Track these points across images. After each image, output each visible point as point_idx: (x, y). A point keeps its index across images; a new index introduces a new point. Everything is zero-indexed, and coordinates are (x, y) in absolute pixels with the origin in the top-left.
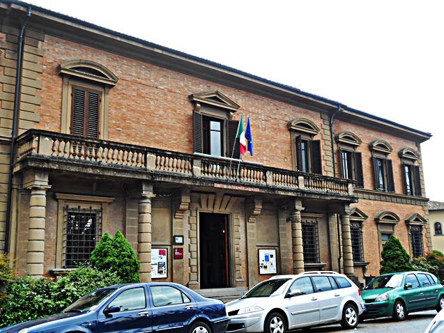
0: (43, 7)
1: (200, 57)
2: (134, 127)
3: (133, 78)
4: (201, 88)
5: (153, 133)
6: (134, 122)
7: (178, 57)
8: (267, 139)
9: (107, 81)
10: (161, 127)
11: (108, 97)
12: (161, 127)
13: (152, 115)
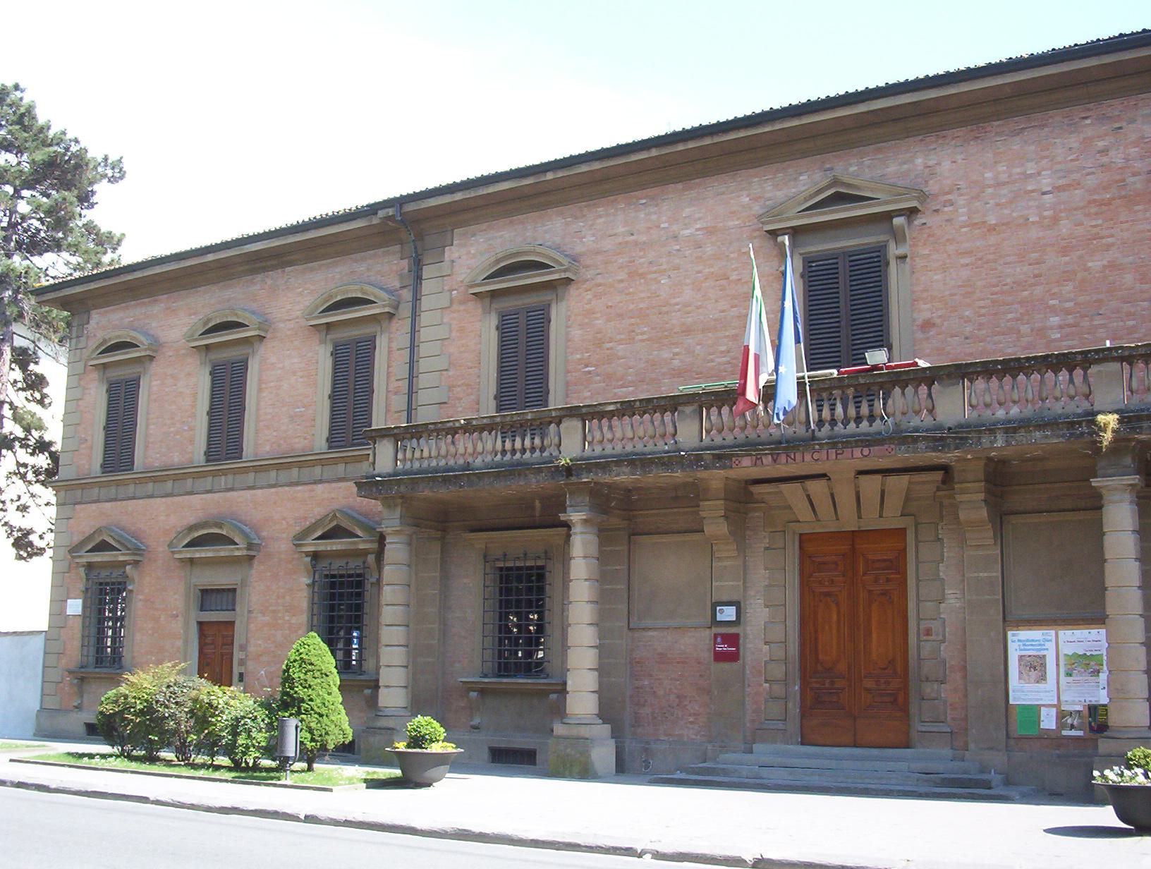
0: (431, 187)
1: (537, 163)
2: (620, 354)
3: (620, 240)
4: (792, 187)
5: (666, 355)
6: (620, 342)
7: (778, 126)
8: (1065, 251)
9: (879, 205)
10: (687, 331)
11: (563, 306)
12: (687, 331)
13: (664, 309)
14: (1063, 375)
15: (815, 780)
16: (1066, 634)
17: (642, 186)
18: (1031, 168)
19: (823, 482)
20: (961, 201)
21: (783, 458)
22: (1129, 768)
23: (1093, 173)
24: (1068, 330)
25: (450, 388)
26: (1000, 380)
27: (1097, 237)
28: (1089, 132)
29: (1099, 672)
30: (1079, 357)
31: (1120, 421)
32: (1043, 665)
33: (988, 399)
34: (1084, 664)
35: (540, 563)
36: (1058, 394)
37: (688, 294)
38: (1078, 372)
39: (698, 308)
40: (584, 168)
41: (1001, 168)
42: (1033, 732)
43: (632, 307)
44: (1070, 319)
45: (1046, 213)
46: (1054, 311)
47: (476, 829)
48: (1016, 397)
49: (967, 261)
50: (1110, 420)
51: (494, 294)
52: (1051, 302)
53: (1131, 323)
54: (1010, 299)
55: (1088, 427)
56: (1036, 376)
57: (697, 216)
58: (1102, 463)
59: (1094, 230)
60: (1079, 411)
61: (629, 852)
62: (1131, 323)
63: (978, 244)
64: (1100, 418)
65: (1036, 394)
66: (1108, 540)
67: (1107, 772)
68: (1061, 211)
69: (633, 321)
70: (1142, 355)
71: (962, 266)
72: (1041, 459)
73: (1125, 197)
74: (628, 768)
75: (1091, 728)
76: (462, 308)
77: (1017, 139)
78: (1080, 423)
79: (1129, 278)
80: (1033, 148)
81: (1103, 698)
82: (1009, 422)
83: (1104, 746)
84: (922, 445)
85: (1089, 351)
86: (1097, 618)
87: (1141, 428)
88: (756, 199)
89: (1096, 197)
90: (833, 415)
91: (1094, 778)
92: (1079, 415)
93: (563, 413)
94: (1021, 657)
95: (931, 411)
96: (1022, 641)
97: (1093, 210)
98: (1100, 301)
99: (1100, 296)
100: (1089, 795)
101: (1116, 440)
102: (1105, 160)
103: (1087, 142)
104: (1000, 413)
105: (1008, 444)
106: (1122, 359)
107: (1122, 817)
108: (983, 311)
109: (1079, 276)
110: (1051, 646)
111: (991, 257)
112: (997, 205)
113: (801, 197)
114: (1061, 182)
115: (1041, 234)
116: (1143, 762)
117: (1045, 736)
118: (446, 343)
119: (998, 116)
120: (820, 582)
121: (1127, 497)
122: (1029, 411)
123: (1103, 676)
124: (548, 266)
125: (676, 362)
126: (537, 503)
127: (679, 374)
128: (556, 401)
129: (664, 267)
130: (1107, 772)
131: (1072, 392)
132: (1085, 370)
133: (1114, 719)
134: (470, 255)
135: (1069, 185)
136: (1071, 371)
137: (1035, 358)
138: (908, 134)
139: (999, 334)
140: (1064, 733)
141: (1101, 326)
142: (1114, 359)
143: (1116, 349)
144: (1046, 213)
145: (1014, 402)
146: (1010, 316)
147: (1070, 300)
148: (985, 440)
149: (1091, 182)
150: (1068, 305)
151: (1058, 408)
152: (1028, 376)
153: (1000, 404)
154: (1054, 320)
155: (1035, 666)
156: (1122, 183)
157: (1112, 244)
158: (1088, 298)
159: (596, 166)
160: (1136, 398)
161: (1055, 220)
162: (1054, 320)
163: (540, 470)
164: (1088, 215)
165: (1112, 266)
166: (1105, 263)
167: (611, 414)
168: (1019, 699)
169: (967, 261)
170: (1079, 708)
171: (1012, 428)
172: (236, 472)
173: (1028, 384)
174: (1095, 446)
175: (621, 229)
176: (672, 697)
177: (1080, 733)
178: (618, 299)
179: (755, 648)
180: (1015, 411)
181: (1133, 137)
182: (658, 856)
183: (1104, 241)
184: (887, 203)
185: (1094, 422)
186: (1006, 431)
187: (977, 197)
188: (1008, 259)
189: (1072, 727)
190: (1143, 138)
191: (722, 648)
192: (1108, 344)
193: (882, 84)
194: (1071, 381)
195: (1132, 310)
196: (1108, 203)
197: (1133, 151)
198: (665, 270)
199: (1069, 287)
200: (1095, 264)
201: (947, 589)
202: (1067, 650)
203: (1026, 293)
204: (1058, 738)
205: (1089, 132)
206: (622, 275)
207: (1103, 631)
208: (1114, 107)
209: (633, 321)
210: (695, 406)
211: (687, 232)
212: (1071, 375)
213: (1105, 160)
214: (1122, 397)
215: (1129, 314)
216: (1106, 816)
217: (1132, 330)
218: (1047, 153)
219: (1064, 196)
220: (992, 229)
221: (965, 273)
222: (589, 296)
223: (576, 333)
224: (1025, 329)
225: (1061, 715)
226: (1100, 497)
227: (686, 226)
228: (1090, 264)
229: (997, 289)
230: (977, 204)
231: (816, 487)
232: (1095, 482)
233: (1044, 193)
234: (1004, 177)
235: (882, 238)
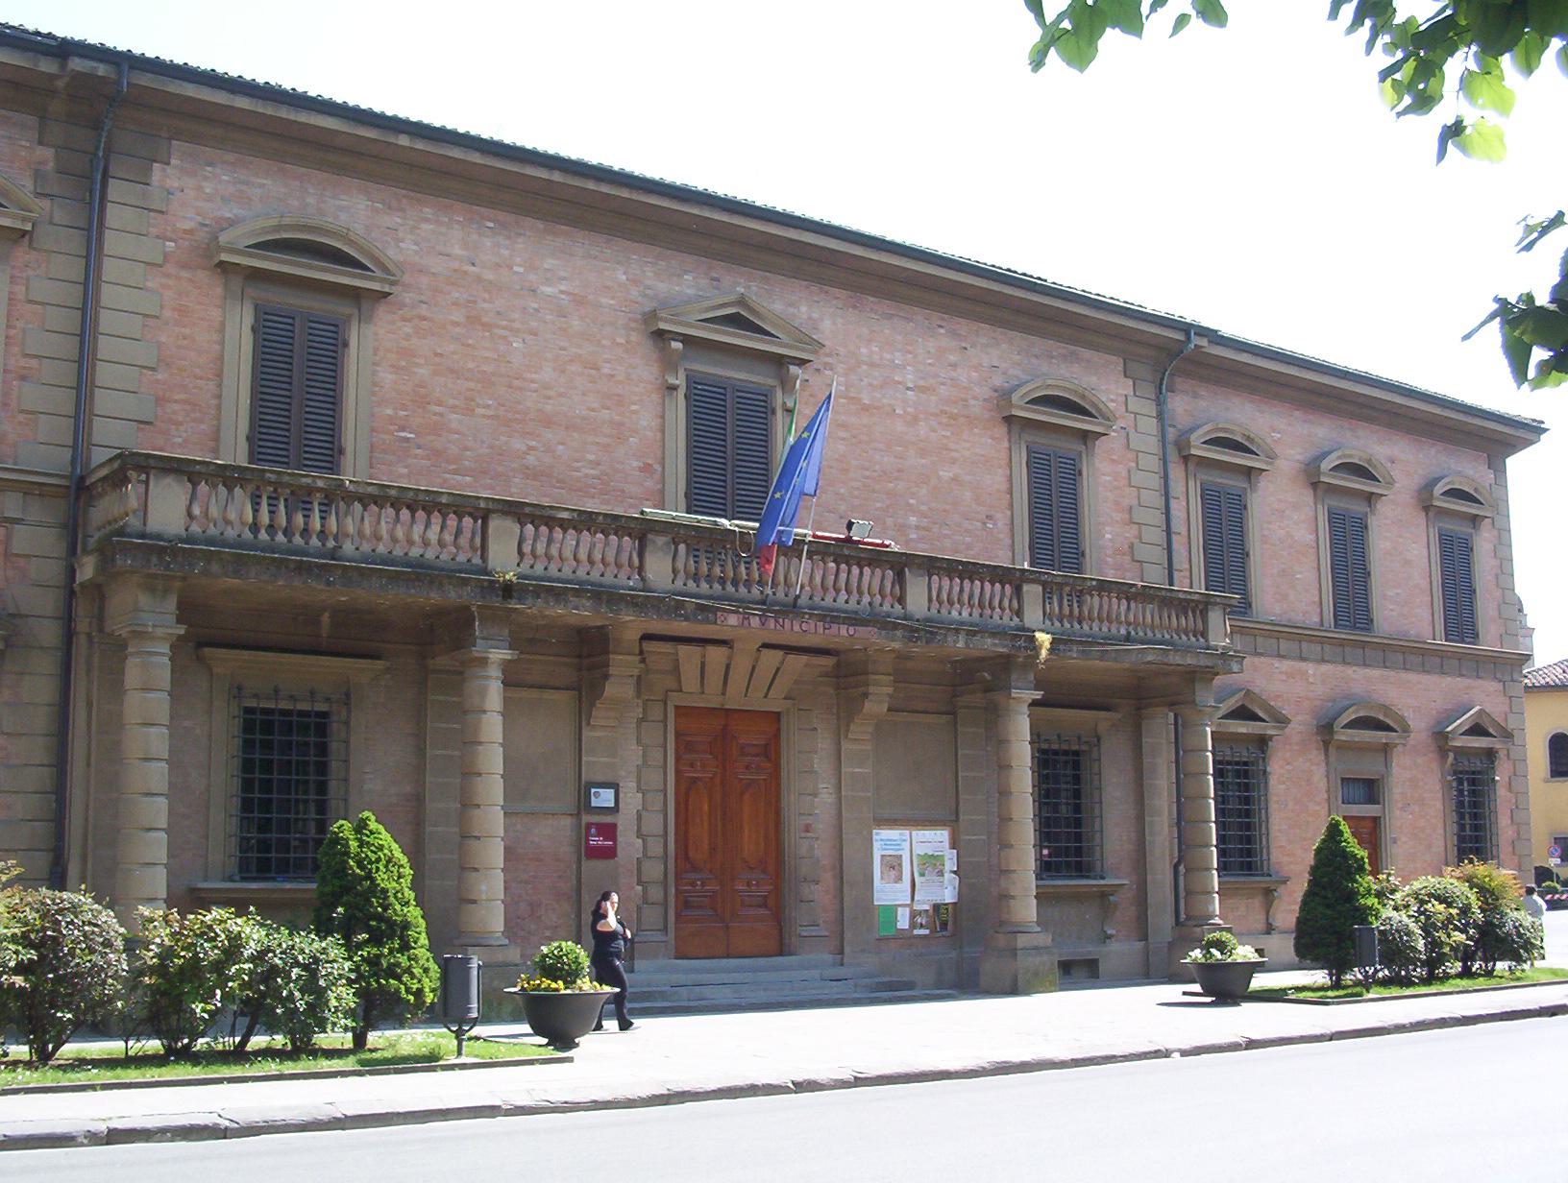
2: (454, 425)
3: (456, 265)
4: (691, 289)
5: (518, 444)
6: (453, 408)
7: (605, 189)
12: (548, 422)
13: (516, 383)
15: (762, 996)
17: (492, 204)
19: (723, 650)
21: (772, 623)
25: (160, 401)
35: (322, 707)
37: (547, 373)
39: (561, 395)
40: (456, 153)
42: (892, 932)
43: (471, 365)
44: (925, 522)
47: (761, 1080)
49: (842, 434)
51: (256, 275)
57: (563, 274)
61: (1157, 1054)
69: (472, 385)
74: (1079, 972)
76: (184, 274)
84: (899, 633)
88: (635, 282)
93: (496, 507)
95: (901, 600)
96: (887, 840)
113: (709, 304)
114: (922, 383)
118: (150, 322)
119: (875, 293)
120: (692, 765)
125: (531, 459)
126: (326, 618)
127: (533, 474)
128: (353, 472)
129: (517, 325)
134: (205, 196)
140: (916, 932)
154: (913, 520)
159: (476, 158)
161: (916, 419)
162: (913, 520)
163: (895, 626)
165: (955, 479)
167: (564, 525)
169: (842, 434)
170: (927, 907)
175: (457, 251)
176: (523, 905)
178: (452, 347)
179: (628, 843)
182: (1184, 1053)
184: (786, 346)
191: (596, 841)
193: (461, 130)
198: (518, 330)
199: (924, 491)
200: (945, 474)
201: (818, 780)
206: (458, 316)
208: (963, 326)
209: (472, 385)
210: (668, 538)
211: (549, 290)
217: (969, 547)
220: (866, 408)
221: (842, 448)
222: (408, 329)
223: (387, 377)
225: (914, 914)
227: (548, 282)
231: (716, 654)
235: (770, 382)
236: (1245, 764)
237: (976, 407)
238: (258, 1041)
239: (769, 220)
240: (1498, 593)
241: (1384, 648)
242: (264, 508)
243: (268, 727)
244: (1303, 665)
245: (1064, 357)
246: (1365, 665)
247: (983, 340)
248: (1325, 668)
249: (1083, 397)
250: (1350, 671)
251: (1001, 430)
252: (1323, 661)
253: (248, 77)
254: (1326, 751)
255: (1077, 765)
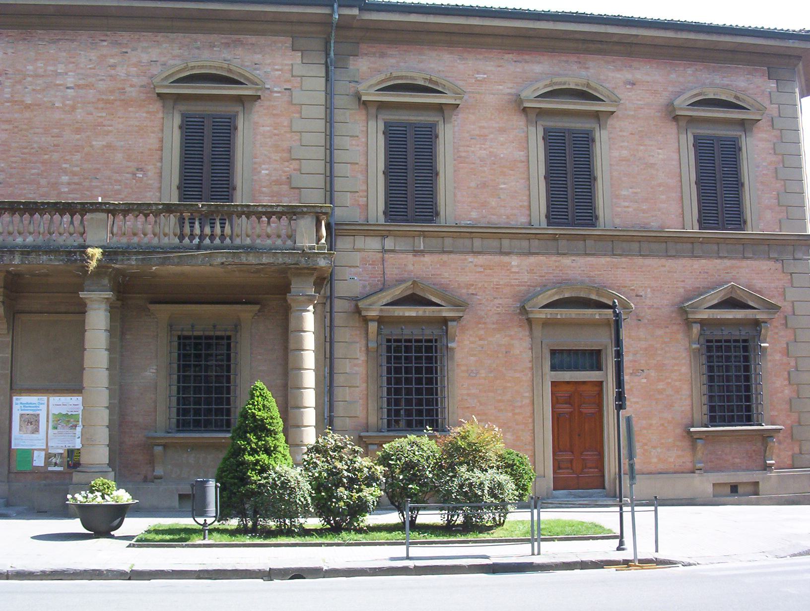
8: (78, 131)
14: (67, 218)
16: (55, 400)
18: (61, 68)
20: (8, 83)
22: (92, 492)
23: (103, 80)
24: (73, 186)
26: (21, 216)
27: (101, 125)
28: (105, 51)
29: (76, 426)
30: (79, 207)
31: (103, 254)
32: (38, 421)
33: (11, 229)
34: (66, 421)
35: (228, 333)
36: (61, 230)
38: (77, 217)
41: (40, 64)
42: (28, 468)
45: (68, 102)
46: (65, 171)
48: (32, 230)
50: (96, 253)
52: (64, 166)
53: (119, 187)
54: (34, 159)
55: (81, 256)
56: (47, 216)
58: (87, 282)
59: (100, 120)
60: (76, 244)
62: (119, 187)
63: (16, 115)
64: (90, 250)
65: (46, 229)
66: (88, 335)
67: (77, 495)
68: (78, 102)
70: (122, 211)
71: (3, 130)
72: (47, 275)
73: (123, 100)
75: (69, 466)
77: (54, 46)
78: (75, 253)
79: (119, 156)
80: (64, 54)
81: (78, 445)
82: (25, 247)
83: (77, 477)
85: (87, 203)
86: (76, 388)
87: (117, 260)
89: (103, 97)
90: (192, 231)
91: (68, 500)
92: (75, 247)
94: (22, 415)
96: (23, 404)
97: (101, 105)
98: (99, 169)
99: (99, 166)
100: (64, 512)
101: (98, 267)
102: (113, 72)
103: (103, 57)
104: (19, 240)
105: (23, 262)
106: (108, 211)
107: (85, 526)
108: (14, 165)
109: (87, 149)
110: (44, 408)
111: (25, 127)
112: (34, 90)
114: (81, 82)
115: (63, 116)
116: (101, 488)
117: (36, 471)
121: (103, 306)
122: (40, 240)
123: (79, 429)
124: (242, 83)
128: (241, 198)
130: (77, 495)
131: (72, 229)
132: (82, 216)
133: (84, 459)
135: (87, 86)
136: (72, 216)
137: (48, 203)
138: (159, 30)
139: (24, 183)
140: (50, 469)
141: (97, 187)
142: (103, 211)
143: (106, 204)
144: (68, 102)
145: (30, 233)
146: (33, 171)
147: (77, 166)
148: (6, 259)
149: (101, 85)
150: (76, 169)
151: (61, 240)
152: (41, 215)
153: (20, 233)
154: (65, 178)
155: (31, 422)
156: (122, 91)
157: (111, 132)
158: (90, 166)
160: (115, 239)
161: (73, 108)
162: (65, 178)
164: (97, 108)
165: (109, 146)
166: (104, 143)
168: (18, 445)
171: (27, 251)
172: (424, 234)
173: (42, 221)
174: (84, 269)
177: (61, 469)
180: (30, 239)
181: (134, 60)
183: (106, 128)
185: (84, 252)
186: (22, 253)
187: (20, 82)
188: (37, 131)
189: (56, 464)
190: (140, 62)
192: (100, 200)
194: (72, 223)
195: (119, 178)
196: (112, 102)
197: (133, 70)
199: (78, 156)
200: (98, 143)
202: (55, 410)
203: (46, 157)
204: (45, 472)
205: (105, 51)
207: (80, 398)
212: (72, 218)
213: (113, 72)
214: (105, 237)
215: (116, 181)
216: (75, 525)
217: (118, 192)
218: (73, 60)
219: (82, 92)
220: (28, 107)
224: (43, 182)
225: (48, 456)
226: (85, 305)
228: (94, 143)
229: (25, 151)
230: (19, 87)
232: (82, 295)
233: (68, 88)
234: (41, 72)
236: (430, 341)
237: (132, 92)
238: (426, 518)
239: (410, 13)
240: (779, 185)
241: (612, 238)
242: (197, 225)
243: (429, 349)
244: (505, 259)
245: (227, 45)
246: (586, 254)
247: (145, 44)
248: (532, 259)
249: (230, 71)
250: (567, 261)
251: (157, 106)
252: (530, 254)
253: (728, 24)
254: (531, 329)
255: (746, 349)
